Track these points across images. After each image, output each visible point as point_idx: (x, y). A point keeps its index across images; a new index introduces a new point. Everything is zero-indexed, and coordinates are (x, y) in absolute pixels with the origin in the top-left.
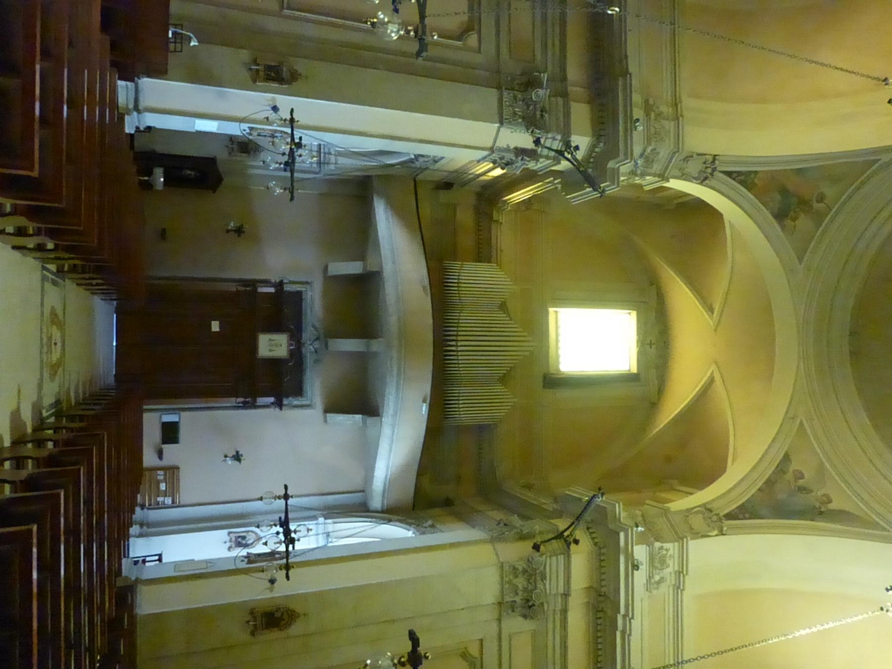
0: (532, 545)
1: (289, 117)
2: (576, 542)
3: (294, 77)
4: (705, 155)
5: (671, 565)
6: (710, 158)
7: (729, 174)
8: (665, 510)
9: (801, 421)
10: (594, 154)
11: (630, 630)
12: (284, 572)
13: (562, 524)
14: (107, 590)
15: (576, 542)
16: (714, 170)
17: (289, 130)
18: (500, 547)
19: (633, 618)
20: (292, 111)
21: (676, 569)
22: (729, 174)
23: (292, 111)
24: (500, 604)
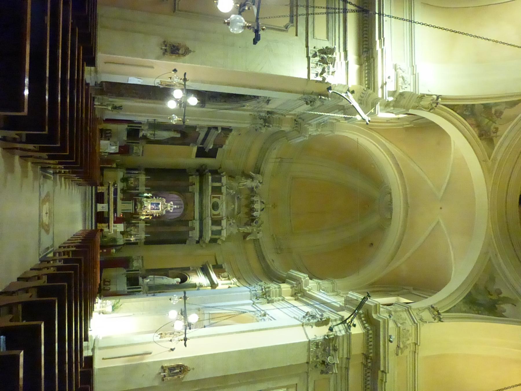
0: (328, 328)
1: (183, 77)
2: (354, 325)
3: (187, 51)
4: (432, 95)
5: (410, 340)
6: (435, 97)
7: (447, 312)
8: (408, 308)
9: (490, 258)
10: (362, 315)
11: (386, 380)
12: (183, 342)
13: (346, 314)
14: (83, 296)
15: (354, 325)
16: (437, 104)
17: (183, 83)
18: (308, 329)
19: (386, 382)
20: (185, 74)
21: (413, 341)
22: (447, 312)
23: (185, 74)
24: (308, 363)
